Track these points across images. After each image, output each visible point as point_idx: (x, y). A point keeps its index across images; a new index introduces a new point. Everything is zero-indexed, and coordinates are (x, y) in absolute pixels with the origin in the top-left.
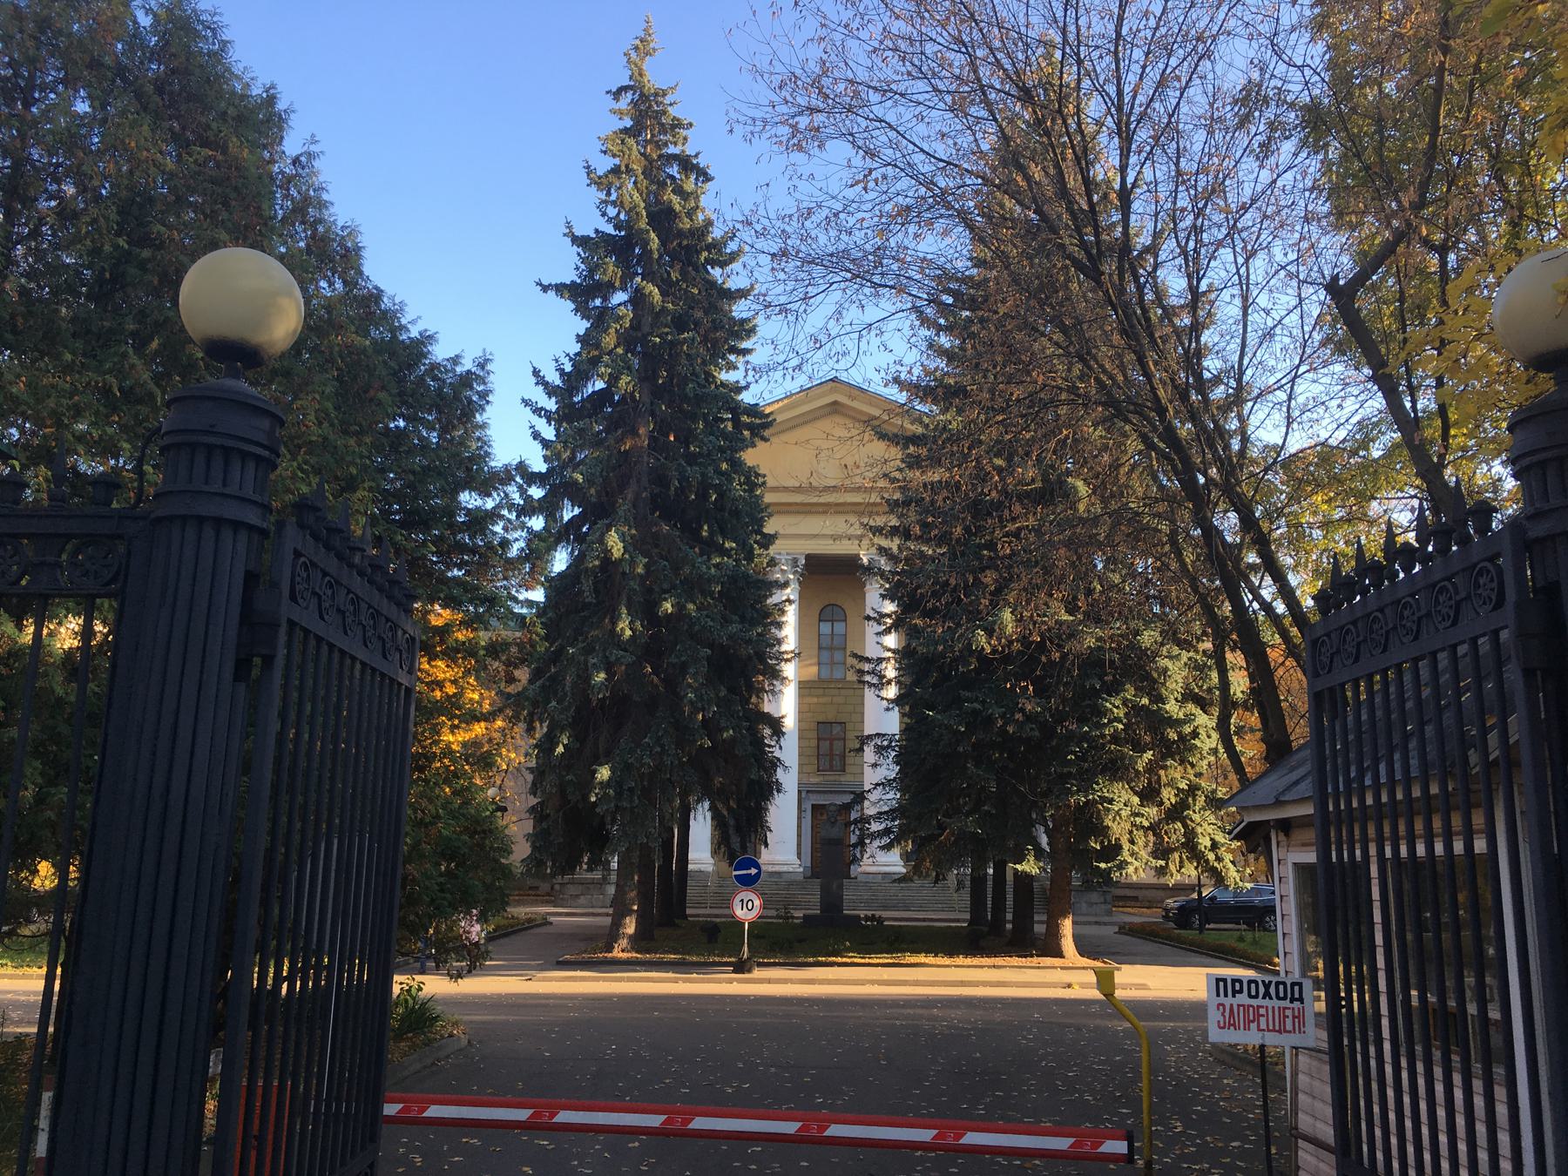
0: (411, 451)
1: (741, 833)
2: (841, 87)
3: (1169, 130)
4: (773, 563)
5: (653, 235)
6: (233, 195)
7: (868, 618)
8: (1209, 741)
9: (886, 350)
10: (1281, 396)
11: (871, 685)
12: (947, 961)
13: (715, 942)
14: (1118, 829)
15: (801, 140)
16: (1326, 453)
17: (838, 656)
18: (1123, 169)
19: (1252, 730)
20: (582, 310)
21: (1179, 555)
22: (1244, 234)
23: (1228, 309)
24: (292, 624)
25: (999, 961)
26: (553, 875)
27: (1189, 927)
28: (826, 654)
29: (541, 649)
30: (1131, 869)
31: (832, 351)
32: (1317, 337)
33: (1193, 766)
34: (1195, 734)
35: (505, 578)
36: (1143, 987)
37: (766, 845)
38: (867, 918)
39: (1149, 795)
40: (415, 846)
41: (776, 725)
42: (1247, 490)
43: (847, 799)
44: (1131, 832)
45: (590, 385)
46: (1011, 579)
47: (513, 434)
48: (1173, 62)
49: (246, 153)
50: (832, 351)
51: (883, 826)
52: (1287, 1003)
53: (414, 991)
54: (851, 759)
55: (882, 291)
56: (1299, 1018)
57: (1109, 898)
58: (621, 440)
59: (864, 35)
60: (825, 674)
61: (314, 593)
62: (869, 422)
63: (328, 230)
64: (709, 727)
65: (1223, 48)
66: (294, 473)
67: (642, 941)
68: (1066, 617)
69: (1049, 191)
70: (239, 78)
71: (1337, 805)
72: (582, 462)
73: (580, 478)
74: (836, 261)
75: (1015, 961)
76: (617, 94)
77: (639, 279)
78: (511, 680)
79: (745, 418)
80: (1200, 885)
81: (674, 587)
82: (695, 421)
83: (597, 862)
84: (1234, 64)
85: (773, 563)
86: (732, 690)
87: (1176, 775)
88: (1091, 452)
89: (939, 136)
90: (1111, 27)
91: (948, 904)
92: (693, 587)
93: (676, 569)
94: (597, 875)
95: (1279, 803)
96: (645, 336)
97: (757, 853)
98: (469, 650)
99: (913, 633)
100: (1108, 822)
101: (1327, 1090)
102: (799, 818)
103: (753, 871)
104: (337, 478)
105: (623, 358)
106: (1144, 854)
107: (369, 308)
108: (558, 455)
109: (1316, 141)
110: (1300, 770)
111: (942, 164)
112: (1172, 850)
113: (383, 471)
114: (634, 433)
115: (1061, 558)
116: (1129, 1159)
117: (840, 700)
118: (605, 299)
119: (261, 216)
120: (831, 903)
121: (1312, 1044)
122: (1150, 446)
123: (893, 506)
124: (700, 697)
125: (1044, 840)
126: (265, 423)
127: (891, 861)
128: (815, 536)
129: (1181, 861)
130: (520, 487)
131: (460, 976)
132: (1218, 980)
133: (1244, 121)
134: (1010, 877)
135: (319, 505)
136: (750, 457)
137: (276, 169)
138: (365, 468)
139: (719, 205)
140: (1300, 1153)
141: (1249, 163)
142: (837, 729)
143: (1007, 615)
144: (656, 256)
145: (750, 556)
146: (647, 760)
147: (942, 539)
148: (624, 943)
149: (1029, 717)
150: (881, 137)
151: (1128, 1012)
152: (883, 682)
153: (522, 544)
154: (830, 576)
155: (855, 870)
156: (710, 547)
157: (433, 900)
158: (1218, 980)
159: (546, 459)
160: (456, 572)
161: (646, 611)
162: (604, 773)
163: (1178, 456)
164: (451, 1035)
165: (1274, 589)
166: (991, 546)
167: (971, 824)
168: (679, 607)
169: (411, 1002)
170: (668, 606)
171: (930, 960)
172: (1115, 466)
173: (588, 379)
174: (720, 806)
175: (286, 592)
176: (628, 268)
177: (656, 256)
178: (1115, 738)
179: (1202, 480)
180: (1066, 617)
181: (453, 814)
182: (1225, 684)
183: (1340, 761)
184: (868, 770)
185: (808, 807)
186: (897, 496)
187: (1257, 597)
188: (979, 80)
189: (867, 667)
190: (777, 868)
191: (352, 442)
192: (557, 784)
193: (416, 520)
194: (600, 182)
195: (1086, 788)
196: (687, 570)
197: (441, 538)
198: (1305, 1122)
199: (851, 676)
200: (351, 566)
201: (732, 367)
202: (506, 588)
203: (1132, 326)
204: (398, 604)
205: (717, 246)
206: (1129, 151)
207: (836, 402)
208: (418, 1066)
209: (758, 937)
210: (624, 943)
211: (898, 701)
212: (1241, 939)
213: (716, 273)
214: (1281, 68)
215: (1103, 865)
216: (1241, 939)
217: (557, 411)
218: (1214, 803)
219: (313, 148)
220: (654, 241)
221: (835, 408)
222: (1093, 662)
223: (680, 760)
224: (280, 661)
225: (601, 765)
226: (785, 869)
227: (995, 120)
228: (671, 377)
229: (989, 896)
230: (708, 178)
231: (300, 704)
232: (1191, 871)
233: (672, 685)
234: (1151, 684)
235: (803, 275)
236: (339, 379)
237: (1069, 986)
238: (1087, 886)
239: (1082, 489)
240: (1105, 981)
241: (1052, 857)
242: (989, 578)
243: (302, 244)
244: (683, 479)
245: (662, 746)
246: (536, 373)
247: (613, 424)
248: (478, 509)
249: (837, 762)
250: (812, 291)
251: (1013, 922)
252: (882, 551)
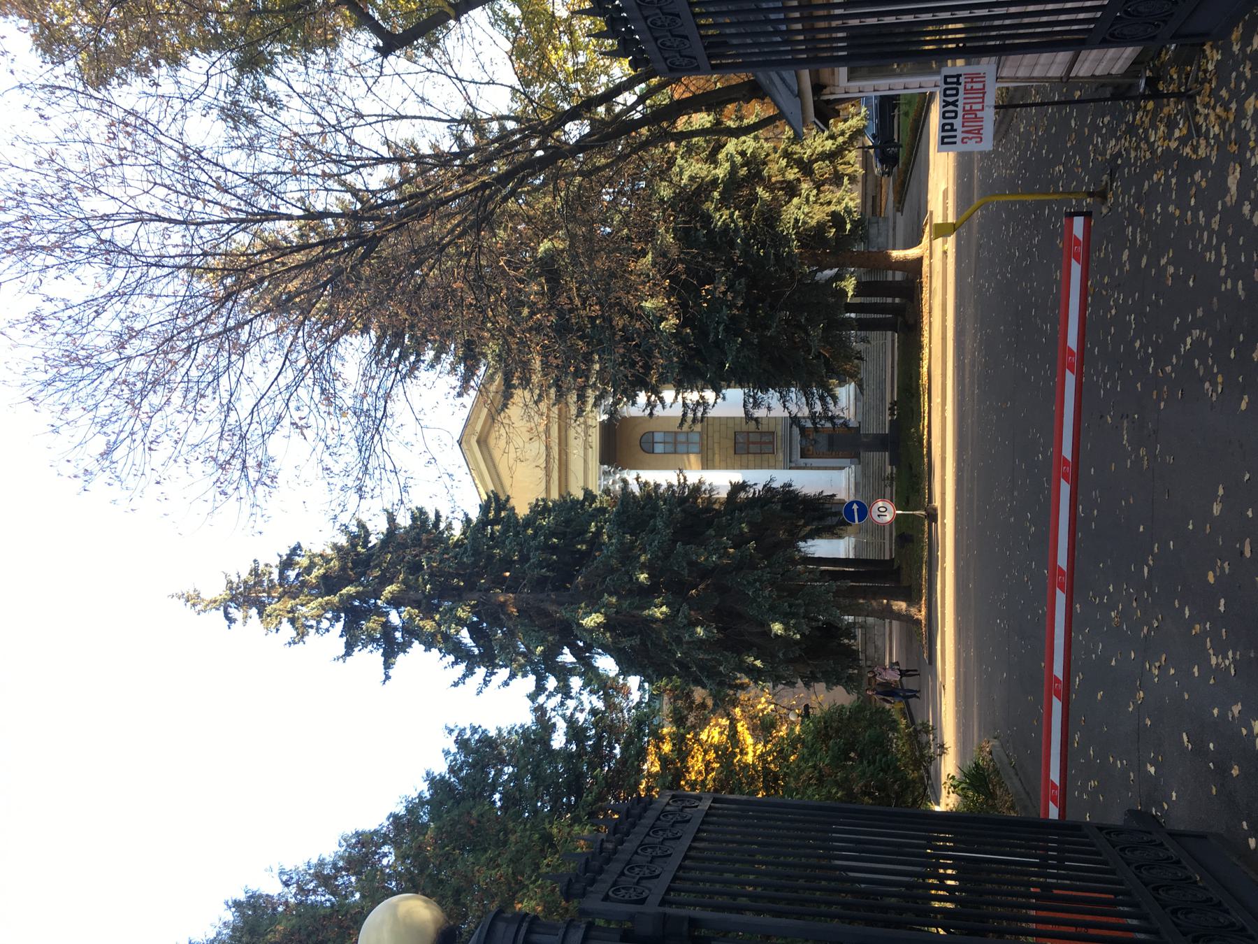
0: (520, 788)
1: (822, 515)
2: (225, 445)
3: (255, 180)
4: (607, 491)
5: (344, 591)
6: (314, 938)
7: (651, 414)
8: (749, 143)
9: (434, 401)
10: (472, 89)
11: (705, 412)
12: (926, 351)
13: (913, 537)
14: (819, 214)
15: (266, 475)
16: (519, 52)
17: (682, 438)
18: (289, 217)
19: (739, 110)
20: (404, 647)
21: (599, 169)
22: (342, 119)
23: (401, 132)
24: (663, 903)
25: (925, 309)
26: (860, 668)
27: (897, 153)
28: (681, 448)
29: (678, 682)
30: (851, 204)
31: (439, 447)
32: (424, 60)
33: (768, 155)
34: (743, 154)
35: (622, 711)
36: (945, 193)
38: (892, 414)
39: (791, 190)
40: (839, 785)
41: (737, 488)
42: (546, 117)
43: (796, 430)
44: (822, 204)
45: (464, 641)
46: (619, 304)
47: (503, 704)
48: (204, 178)
49: (280, 928)
50: (439, 447)
52: (961, 88)
53: (955, 783)
54: (763, 428)
55: (389, 411)
56: (973, 78)
57: (874, 220)
58: (510, 616)
59: (182, 431)
60: (696, 448)
61: (638, 883)
62: (492, 418)
63: (342, 858)
64: (739, 543)
65: (193, 140)
66: (538, 887)
67: (911, 596)
68: (650, 256)
69: (309, 275)
70: (219, 934)
71: (801, 51)
72: (527, 647)
73: (540, 649)
74: (365, 448)
75: (925, 295)
76: (231, 620)
77: (379, 602)
78: (703, 706)
79: (491, 515)
80: (863, 147)
81: (627, 572)
82: (493, 556)
83: (849, 631)
84: (206, 131)
85: (607, 491)
86: (709, 524)
87: (776, 168)
88: (517, 239)
89: (265, 361)
90: (177, 228)
91: (881, 348)
92: (627, 556)
93: (612, 571)
94: (859, 632)
95: (800, 95)
96: (425, 597)
97: (842, 502)
98: (679, 740)
99: (663, 380)
100: (813, 223)
101: (1029, 58)
102: (812, 468)
103: (855, 507)
104: (542, 850)
105: (443, 614)
106: (839, 194)
107: (404, 826)
108: (522, 667)
109: (267, 61)
110: (770, 77)
111: (287, 363)
112: (836, 171)
113: (536, 812)
114: (503, 605)
115: (601, 263)
116: (1087, 215)
117: (716, 436)
118: (395, 629)
119: (331, 915)
120: (880, 443)
121: (995, 67)
122: (513, 193)
123: (561, 395)
124: (716, 551)
125: (828, 273)
126: (501, 926)
127: (846, 394)
128: (585, 461)
129: (845, 163)
130: (548, 697)
131: (942, 746)
133: (251, 120)
134: (858, 300)
135: (566, 879)
136: (522, 510)
137: (292, 901)
138: (534, 827)
139: (322, 539)
140: (1081, 74)
141: (284, 116)
143: (648, 305)
144: (361, 589)
145: (602, 510)
146: (767, 593)
147: (588, 359)
148: (913, 611)
149: (731, 286)
150: (267, 412)
151: (966, 213)
152: (703, 403)
153: (594, 698)
154: (617, 445)
155: (853, 424)
156: (595, 542)
157: (882, 770)
158: (943, 143)
159: (524, 676)
160: (617, 751)
161: (646, 594)
162: (777, 628)
163: (521, 172)
164: (991, 753)
165: (626, 94)
166: (592, 319)
167: (816, 333)
168: (643, 567)
169: (964, 785)
170: (643, 577)
171: (925, 364)
172: (529, 220)
173: (460, 642)
174: (802, 534)
175: (638, 908)
176: (370, 611)
177: (361, 589)
178: (746, 217)
179: (540, 153)
180: (650, 256)
181: (813, 754)
182: (702, 132)
183: (762, 40)
184: (773, 414)
185: (802, 462)
186: (553, 391)
187: (633, 107)
188: (219, 334)
189: (690, 415)
190: (852, 486)
191: (513, 838)
192: (787, 665)
193: (575, 784)
194: (302, 634)
195: (786, 240)
196: (613, 562)
197: (589, 764)
198: (1056, 71)
199: (698, 427)
200: (615, 851)
201: (449, 527)
202: (629, 711)
203: (417, 209)
204: (645, 810)
205: (353, 539)
206: (276, 213)
207: (478, 440)
208: (1016, 780)
209: (908, 502)
210: (913, 611)
211: (717, 390)
212: (906, 114)
213: (373, 540)
214: (210, 91)
215: (848, 226)
216: (906, 114)
218: (797, 138)
219: (276, 871)
220: (349, 590)
221: (483, 442)
222: (685, 236)
223: (766, 567)
224: (697, 912)
225: (770, 630)
226: (852, 480)
227: (251, 320)
228: (458, 576)
229: (873, 316)
230: (299, 547)
231: (725, 882)
232: (853, 155)
233: (705, 573)
234: (703, 188)
235: (377, 472)
236: (462, 849)
237: (945, 252)
238: (865, 238)
239: (545, 245)
240: (942, 231)
241: (842, 266)
242: (619, 322)
243: (353, 879)
244: (540, 565)
245: (755, 581)
246: (456, 684)
247: (496, 621)
248: (566, 734)
249: (765, 439)
250: (389, 467)
251: (894, 297)
252: (598, 399)
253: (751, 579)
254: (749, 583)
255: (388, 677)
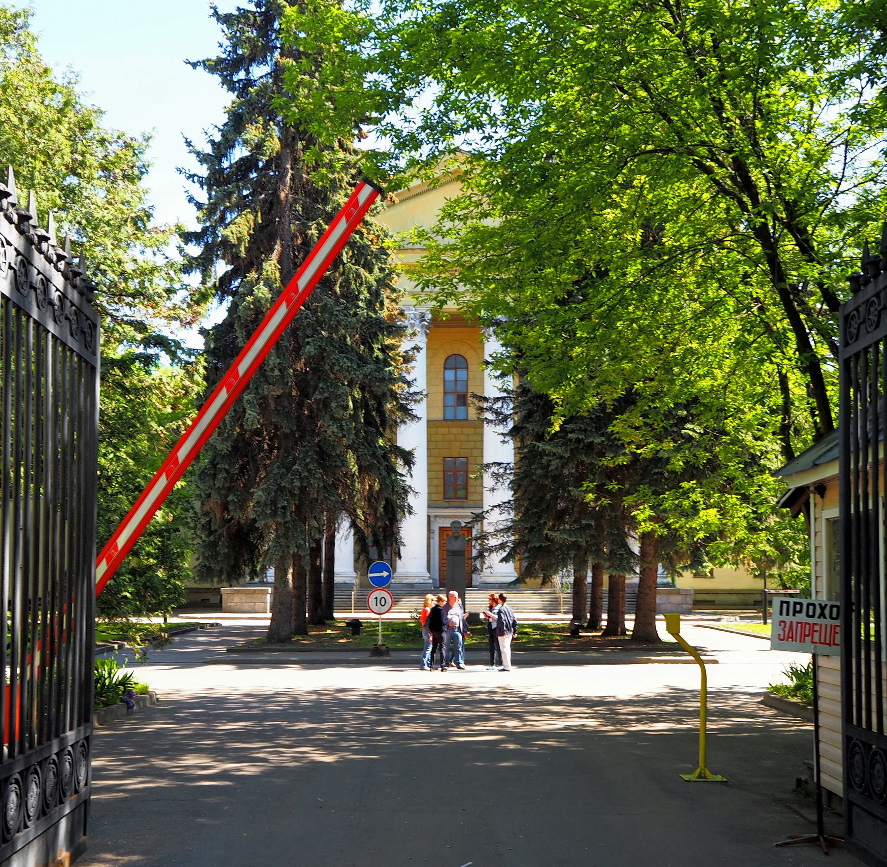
1: (379, 543)
20: (231, 85)
37: (400, 557)
47: (173, 197)
51: (500, 542)
102: (429, 538)
132: (782, 602)
142: (461, 493)
189: (485, 405)
199: (472, 413)
217: (208, 178)
226: (416, 581)
245: (309, 471)
246: (189, 144)
251: (608, 620)
253: (311, 466)
254: (307, 464)
255: (194, 65)
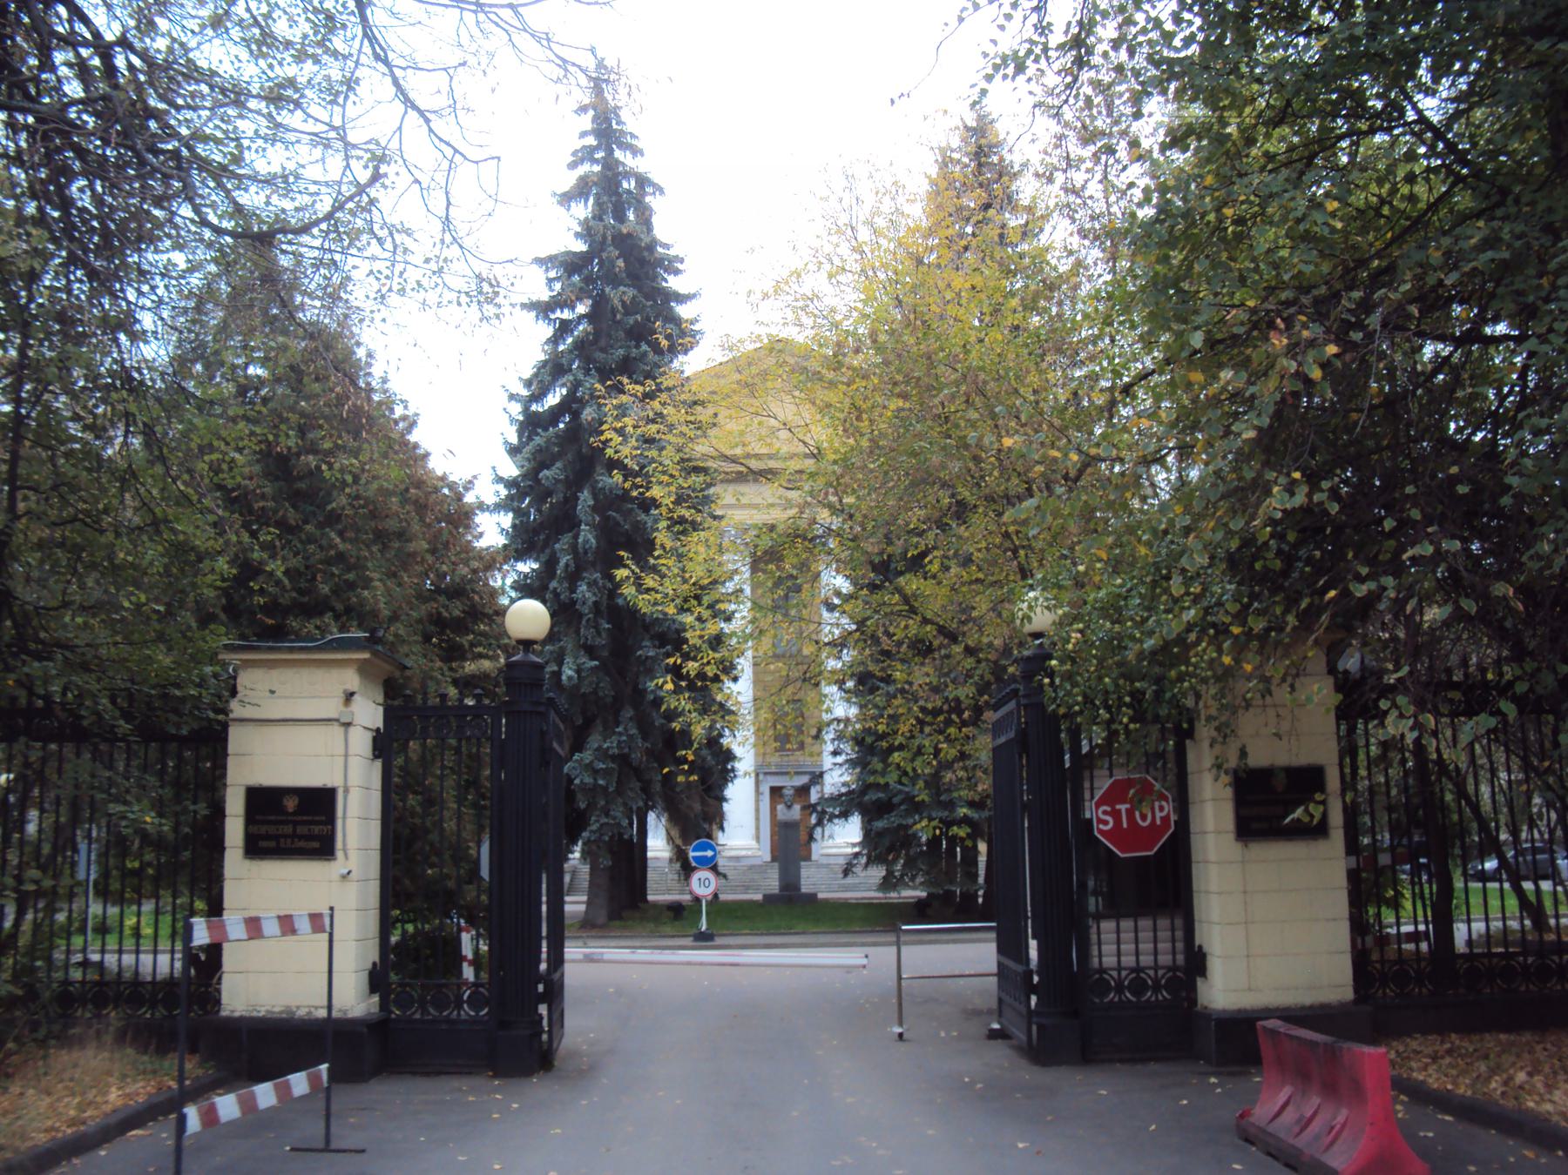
1: (698, 818)
43: (804, 780)
47: (492, 531)
103: (709, 853)
136: (580, 247)
226: (743, 853)
